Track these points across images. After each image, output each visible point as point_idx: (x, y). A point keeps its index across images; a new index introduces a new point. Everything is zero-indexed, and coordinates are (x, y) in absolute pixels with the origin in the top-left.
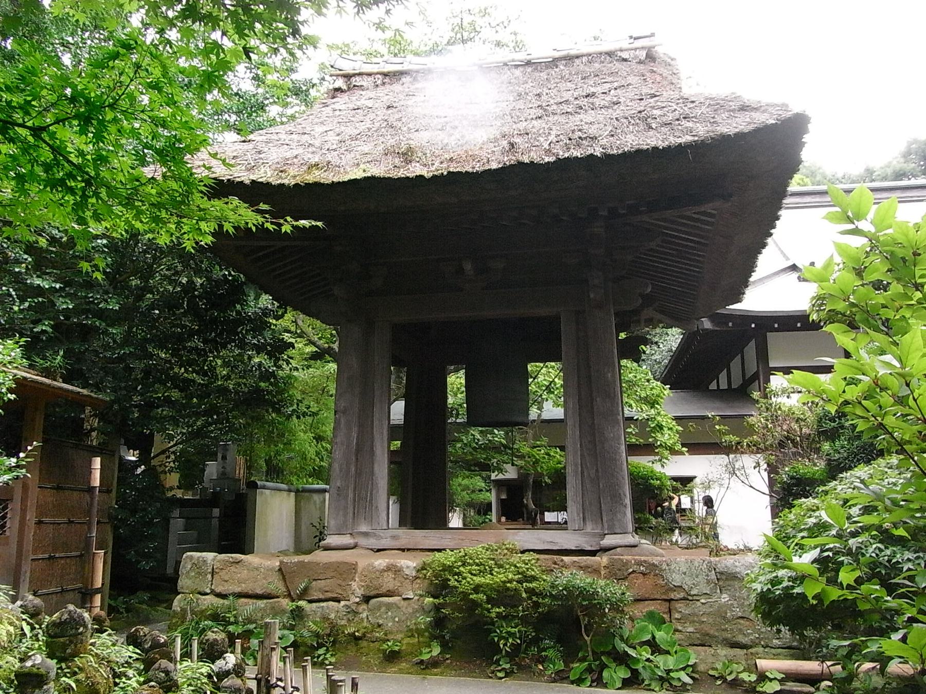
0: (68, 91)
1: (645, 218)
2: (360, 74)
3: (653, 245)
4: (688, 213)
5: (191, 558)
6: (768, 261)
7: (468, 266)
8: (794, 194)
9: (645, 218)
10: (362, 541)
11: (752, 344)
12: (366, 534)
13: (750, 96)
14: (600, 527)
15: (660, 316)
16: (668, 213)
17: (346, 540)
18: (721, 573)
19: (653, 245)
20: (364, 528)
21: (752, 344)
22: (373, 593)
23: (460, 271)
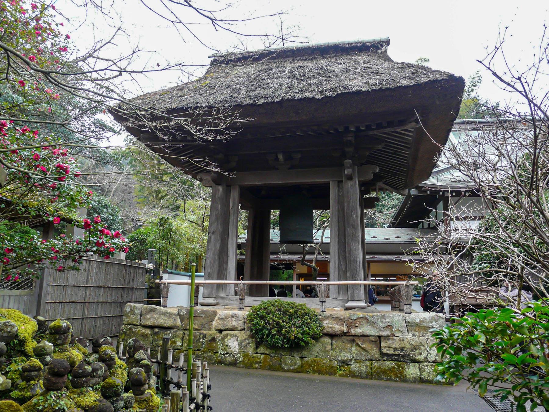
0: (500, 347)
1: (375, 132)
2: (115, 77)
3: (380, 147)
4: (398, 130)
5: (131, 306)
6: (445, 159)
7: (281, 157)
8: (458, 123)
9: (375, 132)
10: (220, 301)
11: (441, 203)
12: (223, 298)
13: (442, 69)
14: (347, 297)
15: (387, 187)
16: (387, 130)
17: (212, 301)
18: (409, 322)
19: (380, 147)
20: (222, 295)
21: (441, 203)
22: (223, 328)
23: (277, 159)
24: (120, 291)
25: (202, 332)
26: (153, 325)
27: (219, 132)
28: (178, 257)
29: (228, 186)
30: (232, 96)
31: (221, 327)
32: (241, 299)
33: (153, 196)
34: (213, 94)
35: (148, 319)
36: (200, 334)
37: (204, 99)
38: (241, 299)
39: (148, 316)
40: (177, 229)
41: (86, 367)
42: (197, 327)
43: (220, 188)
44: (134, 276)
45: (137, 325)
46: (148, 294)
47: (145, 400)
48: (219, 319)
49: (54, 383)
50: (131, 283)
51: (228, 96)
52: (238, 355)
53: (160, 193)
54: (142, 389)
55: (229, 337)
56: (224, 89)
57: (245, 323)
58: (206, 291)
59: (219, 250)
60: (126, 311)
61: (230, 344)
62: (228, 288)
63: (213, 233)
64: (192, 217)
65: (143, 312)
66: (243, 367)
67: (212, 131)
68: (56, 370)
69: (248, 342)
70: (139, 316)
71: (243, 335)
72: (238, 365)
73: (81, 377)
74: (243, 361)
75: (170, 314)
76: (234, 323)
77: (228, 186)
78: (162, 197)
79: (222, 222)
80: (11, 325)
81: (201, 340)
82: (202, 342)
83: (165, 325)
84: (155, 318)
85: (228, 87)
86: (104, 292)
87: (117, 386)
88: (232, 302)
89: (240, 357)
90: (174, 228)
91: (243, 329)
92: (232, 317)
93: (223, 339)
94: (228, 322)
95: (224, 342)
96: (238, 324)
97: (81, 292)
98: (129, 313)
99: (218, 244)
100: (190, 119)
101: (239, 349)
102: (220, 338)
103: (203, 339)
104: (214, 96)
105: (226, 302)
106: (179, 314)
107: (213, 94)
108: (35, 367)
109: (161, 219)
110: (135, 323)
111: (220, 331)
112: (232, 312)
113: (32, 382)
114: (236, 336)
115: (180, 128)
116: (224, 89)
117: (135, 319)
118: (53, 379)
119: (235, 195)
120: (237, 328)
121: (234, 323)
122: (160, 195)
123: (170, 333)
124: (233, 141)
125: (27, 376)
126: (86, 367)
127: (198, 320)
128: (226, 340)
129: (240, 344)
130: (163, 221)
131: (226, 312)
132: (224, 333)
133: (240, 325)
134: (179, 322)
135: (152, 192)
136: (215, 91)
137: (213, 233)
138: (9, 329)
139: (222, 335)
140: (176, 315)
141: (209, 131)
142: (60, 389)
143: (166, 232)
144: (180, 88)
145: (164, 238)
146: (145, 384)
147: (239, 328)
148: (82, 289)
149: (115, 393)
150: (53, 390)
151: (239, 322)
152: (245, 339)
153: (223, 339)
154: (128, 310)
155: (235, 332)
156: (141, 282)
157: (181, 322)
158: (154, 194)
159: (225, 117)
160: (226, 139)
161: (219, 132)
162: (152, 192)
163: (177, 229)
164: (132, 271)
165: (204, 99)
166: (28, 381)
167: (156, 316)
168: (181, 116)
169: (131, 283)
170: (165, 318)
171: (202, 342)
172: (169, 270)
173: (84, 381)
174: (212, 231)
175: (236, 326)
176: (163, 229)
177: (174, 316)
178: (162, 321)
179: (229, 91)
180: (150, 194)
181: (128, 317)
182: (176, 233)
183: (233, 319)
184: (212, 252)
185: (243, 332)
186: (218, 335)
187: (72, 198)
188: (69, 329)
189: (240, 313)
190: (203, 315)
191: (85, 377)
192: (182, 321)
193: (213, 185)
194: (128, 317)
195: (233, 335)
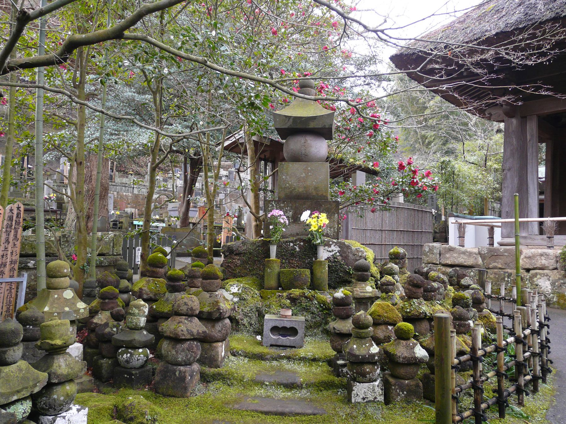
5: (429, 246)
22: (531, 267)
24: (411, 234)
25: (506, 271)
26: (453, 263)
27: (544, 54)
28: (464, 200)
29: (524, 119)
30: (527, 14)
31: (528, 266)
32: (549, 238)
33: (419, 143)
34: (502, 17)
35: (448, 258)
36: (505, 272)
37: (492, 26)
38: (549, 238)
39: (448, 256)
40: (459, 171)
41: (433, 284)
42: (500, 266)
43: (514, 121)
44: (422, 221)
45: (437, 264)
46: (433, 239)
47: (485, 317)
48: (525, 257)
49: (415, 293)
50: (420, 226)
51: (521, 16)
52: (551, 295)
53: (426, 138)
54: (481, 306)
55: (538, 276)
56: (515, 8)
57: (557, 262)
58: (504, 231)
59: (517, 187)
60: (425, 251)
61: (540, 284)
62: (530, 226)
63: (509, 170)
64: (472, 159)
65: (443, 252)
66: (558, 308)
67: (535, 54)
68: (415, 282)
69: (562, 281)
70: (438, 256)
71: (555, 275)
72: (552, 306)
73: (430, 292)
74: (558, 302)
75: (470, 254)
76: (544, 262)
77: (524, 119)
78: (430, 143)
79: (518, 157)
80: (361, 251)
81: (506, 279)
82: (508, 281)
83: (465, 264)
84: (455, 257)
85: (520, 5)
86: (397, 235)
87: (467, 298)
88: (536, 242)
89: (553, 297)
90: (456, 171)
91: (556, 269)
92: (542, 255)
93: (531, 278)
94: (537, 260)
95: (534, 281)
96: (551, 263)
97: (378, 235)
98: (428, 252)
99: (516, 181)
100: (511, 47)
101: (552, 289)
102: (528, 277)
103: (508, 278)
104: (504, 19)
105: (529, 241)
106: (479, 253)
107: (502, 17)
108: (391, 282)
109: (443, 162)
110: (434, 262)
111: (528, 270)
112: (540, 251)
113: (390, 294)
114: (547, 275)
115: (499, 59)
116: (515, 8)
117: (435, 258)
118: (414, 289)
119: (532, 127)
120: (548, 267)
121: (543, 261)
122: (427, 141)
123: (472, 271)
124: (558, 59)
125: (386, 288)
126: (433, 284)
127: (500, 259)
128: (535, 279)
129: (553, 284)
130: (444, 165)
131: (533, 250)
132: (532, 272)
133: (552, 264)
134: (480, 261)
135: (419, 139)
136: (504, 13)
137: (509, 170)
138: (360, 254)
139: (530, 274)
140: (476, 254)
141: (531, 55)
142: (419, 298)
143: (450, 176)
144: (462, 19)
145: (447, 181)
146: (483, 303)
147: (551, 267)
148: (379, 232)
149: (466, 305)
150: (415, 298)
151: (551, 261)
152: (559, 279)
153: (531, 278)
154: (427, 250)
155: (545, 271)
156: (428, 226)
157: (483, 261)
158: (420, 140)
159: (551, 36)
160: (549, 60)
161: (544, 54)
162: (419, 139)
163: (459, 171)
164: (420, 216)
165: (492, 26)
166: (387, 293)
167: (455, 255)
168: (501, 46)
169: (420, 226)
170: (466, 257)
171: (508, 281)
172: (455, 214)
173: (433, 295)
174: (507, 168)
175: (547, 265)
176: (445, 173)
177: (475, 255)
178: (462, 260)
179: (521, 9)
180: (416, 141)
181: (427, 256)
182: (458, 175)
183: (543, 258)
184: (509, 189)
185: (556, 271)
186: (526, 274)
187: (385, 144)
188: (405, 255)
189: (550, 251)
190: (506, 254)
191: (434, 292)
192: (483, 259)
193: (506, 118)
194: (427, 256)
195: (544, 274)
